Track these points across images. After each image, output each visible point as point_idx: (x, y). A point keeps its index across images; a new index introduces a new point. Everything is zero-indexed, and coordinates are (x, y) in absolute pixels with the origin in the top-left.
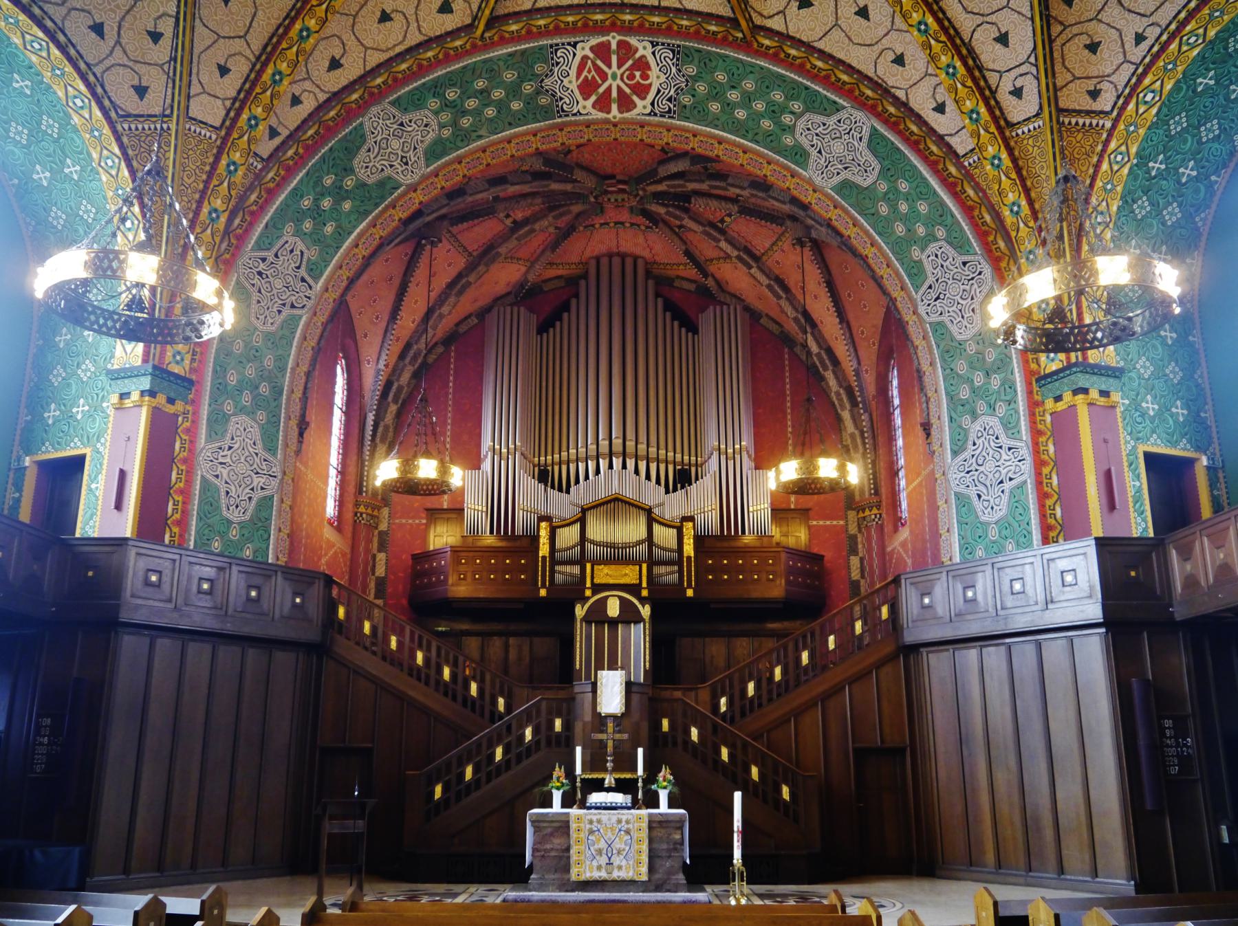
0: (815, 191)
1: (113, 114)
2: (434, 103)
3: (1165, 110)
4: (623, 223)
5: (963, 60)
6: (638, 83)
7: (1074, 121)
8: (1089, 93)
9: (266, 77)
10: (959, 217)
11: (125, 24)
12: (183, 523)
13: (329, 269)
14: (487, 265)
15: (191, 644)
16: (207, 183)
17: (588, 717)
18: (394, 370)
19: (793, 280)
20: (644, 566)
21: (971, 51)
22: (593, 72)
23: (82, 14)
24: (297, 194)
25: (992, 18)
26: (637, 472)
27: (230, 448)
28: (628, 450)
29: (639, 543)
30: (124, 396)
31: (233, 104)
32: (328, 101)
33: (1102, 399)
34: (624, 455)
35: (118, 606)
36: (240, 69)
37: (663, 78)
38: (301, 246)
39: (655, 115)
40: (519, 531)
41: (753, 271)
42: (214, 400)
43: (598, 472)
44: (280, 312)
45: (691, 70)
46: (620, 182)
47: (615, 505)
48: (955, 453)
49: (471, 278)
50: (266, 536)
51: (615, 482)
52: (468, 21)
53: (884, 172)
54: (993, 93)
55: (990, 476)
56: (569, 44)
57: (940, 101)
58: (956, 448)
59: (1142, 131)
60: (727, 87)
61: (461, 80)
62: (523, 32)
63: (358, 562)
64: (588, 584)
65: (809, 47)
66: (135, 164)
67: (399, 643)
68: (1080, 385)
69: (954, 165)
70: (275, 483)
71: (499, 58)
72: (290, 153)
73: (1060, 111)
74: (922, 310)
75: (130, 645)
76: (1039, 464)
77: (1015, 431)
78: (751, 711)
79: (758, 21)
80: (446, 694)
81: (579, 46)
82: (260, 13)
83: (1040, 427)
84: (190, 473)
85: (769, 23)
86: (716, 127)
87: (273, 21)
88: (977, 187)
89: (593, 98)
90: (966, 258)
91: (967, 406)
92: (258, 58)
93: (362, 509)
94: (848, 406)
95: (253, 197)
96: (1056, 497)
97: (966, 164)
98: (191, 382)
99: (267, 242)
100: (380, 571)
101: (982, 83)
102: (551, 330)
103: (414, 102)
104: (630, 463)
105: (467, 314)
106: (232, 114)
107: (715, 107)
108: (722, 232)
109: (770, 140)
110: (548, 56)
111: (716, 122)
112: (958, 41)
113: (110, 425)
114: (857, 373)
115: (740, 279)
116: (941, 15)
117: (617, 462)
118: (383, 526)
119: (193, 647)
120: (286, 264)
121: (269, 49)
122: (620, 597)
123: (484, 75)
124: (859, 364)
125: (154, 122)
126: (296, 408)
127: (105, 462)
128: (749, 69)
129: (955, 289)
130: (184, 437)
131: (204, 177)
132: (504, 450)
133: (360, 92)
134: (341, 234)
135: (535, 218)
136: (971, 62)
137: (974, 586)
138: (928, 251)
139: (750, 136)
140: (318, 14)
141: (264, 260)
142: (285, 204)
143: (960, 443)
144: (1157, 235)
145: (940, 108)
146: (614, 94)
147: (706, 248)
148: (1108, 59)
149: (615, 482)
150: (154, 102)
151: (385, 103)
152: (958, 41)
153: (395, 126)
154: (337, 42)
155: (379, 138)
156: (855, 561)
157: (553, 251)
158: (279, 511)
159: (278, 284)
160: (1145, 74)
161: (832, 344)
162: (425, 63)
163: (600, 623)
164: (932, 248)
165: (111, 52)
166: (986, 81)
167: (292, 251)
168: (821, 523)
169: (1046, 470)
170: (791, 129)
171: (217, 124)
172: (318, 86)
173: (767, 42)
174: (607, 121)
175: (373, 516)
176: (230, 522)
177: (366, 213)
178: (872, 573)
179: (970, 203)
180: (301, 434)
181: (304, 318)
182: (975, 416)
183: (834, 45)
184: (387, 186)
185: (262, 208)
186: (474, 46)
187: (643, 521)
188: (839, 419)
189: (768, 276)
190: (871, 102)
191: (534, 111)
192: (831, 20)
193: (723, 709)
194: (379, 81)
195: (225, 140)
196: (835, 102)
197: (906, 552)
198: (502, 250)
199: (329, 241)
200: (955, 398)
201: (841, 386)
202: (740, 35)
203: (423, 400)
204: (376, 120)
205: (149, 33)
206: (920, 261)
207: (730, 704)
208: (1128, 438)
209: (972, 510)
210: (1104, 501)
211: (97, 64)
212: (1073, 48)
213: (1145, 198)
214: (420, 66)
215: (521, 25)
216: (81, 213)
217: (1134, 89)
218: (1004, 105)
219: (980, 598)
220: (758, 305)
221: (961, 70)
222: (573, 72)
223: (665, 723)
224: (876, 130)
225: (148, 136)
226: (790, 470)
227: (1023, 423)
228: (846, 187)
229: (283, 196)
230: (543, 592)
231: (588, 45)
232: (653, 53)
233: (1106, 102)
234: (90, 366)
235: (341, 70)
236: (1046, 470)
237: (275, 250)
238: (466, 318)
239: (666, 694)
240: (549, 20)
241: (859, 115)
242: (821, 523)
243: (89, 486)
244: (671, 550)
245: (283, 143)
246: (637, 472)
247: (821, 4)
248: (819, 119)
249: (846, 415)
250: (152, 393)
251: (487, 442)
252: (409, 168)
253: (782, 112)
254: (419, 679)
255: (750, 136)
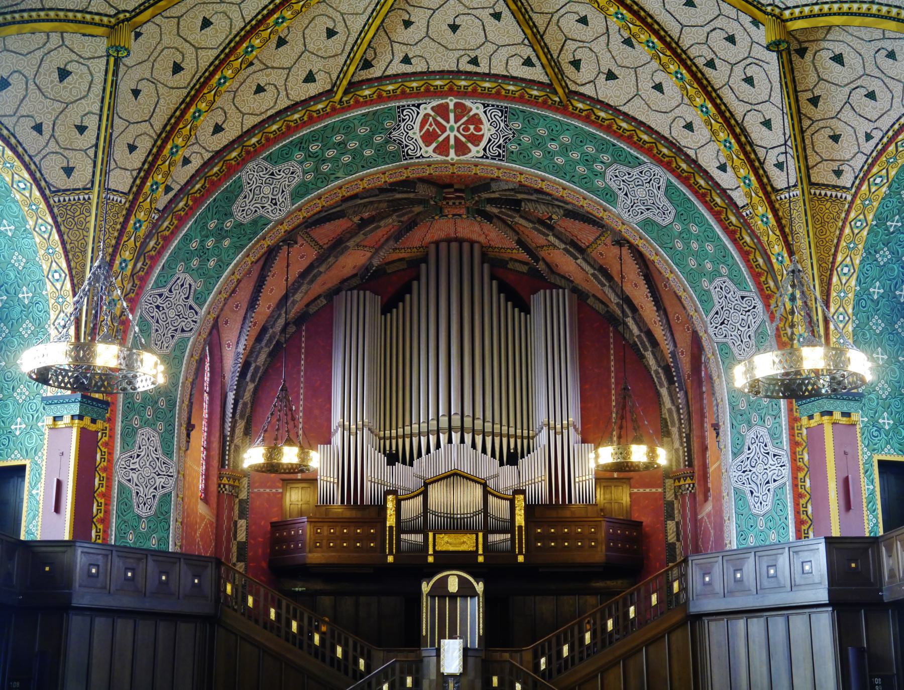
0: (623, 224)
1: (47, 192)
2: (299, 155)
3: (895, 185)
4: (460, 215)
5: (737, 137)
6: (472, 133)
7: (823, 193)
8: (834, 171)
9: (166, 152)
10: (737, 259)
11: (59, 122)
12: (105, 521)
13: (211, 296)
14: (336, 257)
15: (119, 620)
16: (119, 239)
17: (433, 676)
18: (252, 352)
19: (614, 271)
20: (481, 535)
21: (743, 130)
22: (434, 126)
23: (28, 119)
24: (187, 238)
25: (759, 107)
26: (474, 446)
27: (138, 456)
28: (465, 426)
29: (476, 514)
30: (55, 419)
31: (139, 173)
32: (211, 159)
33: (845, 419)
34: (462, 429)
35: (71, 594)
36: (145, 145)
37: (493, 131)
38: (189, 280)
39: (487, 158)
40: (367, 501)
41: (579, 261)
42: (125, 417)
43: (438, 446)
44: (173, 336)
45: (517, 125)
46: (457, 191)
47: (454, 476)
48: (735, 455)
49: (322, 269)
50: (166, 527)
51: (454, 455)
52: (329, 87)
53: (678, 215)
54: (762, 164)
55: (760, 476)
56: (413, 105)
57: (412, 61)
58: (735, 451)
59: (876, 204)
60: (547, 140)
61: (322, 137)
62: (375, 96)
63: (221, 530)
64: (431, 551)
65: (616, 111)
66: (62, 228)
67: (278, 615)
68: (825, 409)
69: (734, 214)
70: (172, 481)
71: (355, 118)
72: (181, 204)
73: (812, 184)
74: (711, 331)
75: (77, 623)
76: (795, 470)
77: (779, 441)
78: (566, 668)
79: (573, 87)
80: (316, 656)
81: (421, 107)
82: (162, 101)
83: (798, 439)
84: (109, 479)
85: (582, 90)
86: (539, 169)
87: (171, 106)
88: (753, 234)
89: (434, 145)
90: (744, 294)
91: (745, 416)
92: (159, 136)
93: (225, 481)
94: (665, 384)
95: (152, 243)
96: (808, 496)
97: (744, 214)
98: (107, 403)
99: (163, 281)
100: (242, 536)
101: (753, 156)
102: (395, 310)
103: (284, 156)
104: (468, 438)
105: (316, 295)
106: (138, 182)
107: (537, 154)
108: (551, 228)
109: (584, 181)
110: (397, 115)
111: (539, 165)
112: (733, 122)
113: (46, 442)
114: (673, 355)
115: (569, 265)
116: (718, 101)
117: (456, 437)
118: (243, 495)
119: (120, 623)
120: (178, 297)
121: (168, 128)
122: (458, 576)
123: (342, 131)
124: (675, 346)
125: (78, 194)
126: (185, 415)
127: (43, 472)
128: (566, 127)
129: (736, 318)
130: (103, 449)
131: (116, 234)
132: (353, 427)
133: (239, 150)
134: (221, 266)
135: (381, 216)
136: (743, 139)
137: (741, 570)
138: (715, 283)
139: (568, 177)
140: (208, 99)
141: (161, 295)
142: (178, 248)
143: (738, 447)
144: (898, 276)
145: (723, 168)
146: (452, 142)
147: (537, 238)
148: (846, 149)
149: (454, 455)
150: (80, 178)
151: (259, 160)
152: (733, 122)
153: (267, 176)
154: (220, 112)
155: (254, 187)
156: (671, 525)
157: (396, 241)
158: (176, 505)
159: (172, 314)
160: (872, 165)
161: (651, 327)
162: (292, 124)
163: (442, 597)
164: (718, 282)
165: (47, 144)
166: (756, 154)
167: (182, 285)
168: (641, 490)
169: (801, 475)
170: (603, 175)
171: (126, 190)
172: (204, 148)
173: (580, 105)
174: (446, 162)
175: (233, 487)
176: (140, 517)
177: (242, 247)
178: (686, 542)
179: (747, 248)
180: (188, 435)
181: (192, 340)
182: (750, 426)
183: (635, 109)
184: (258, 223)
185: (160, 253)
186: (334, 109)
187: (478, 491)
188: (658, 395)
189: (592, 266)
190: (667, 159)
191: (382, 156)
192: (633, 91)
193: (543, 667)
194: (254, 140)
195: (133, 203)
196: (637, 158)
197: (710, 523)
198: (351, 243)
199: (211, 273)
200: (736, 408)
201: (659, 366)
202: (557, 99)
203: (277, 377)
204: (252, 174)
205: (77, 127)
206: (709, 291)
207: (548, 663)
208: (865, 450)
209: (746, 504)
210: (842, 502)
211: (37, 155)
212: (821, 137)
213: (885, 249)
214: (288, 127)
215: (374, 90)
216: (13, 261)
217: (865, 175)
218: (770, 174)
219: (745, 579)
220: (585, 286)
221: (735, 146)
222: (417, 126)
223: (495, 680)
224: (671, 183)
225: (73, 205)
226: (607, 454)
227: (784, 435)
228: (647, 224)
229: (176, 242)
230: (390, 559)
231: (429, 106)
232: (485, 112)
233: (847, 180)
234: (24, 390)
235: (222, 133)
236: (801, 475)
237: (169, 286)
238: (316, 299)
239: (497, 656)
240: (397, 85)
241: (658, 170)
242: (641, 490)
243: (30, 492)
244: (504, 521)
245: (175, 196)
246: (474, 446)
247: (624, 78)
248: (625, 169)
249: (664, 392)
250: (80, 417)
251: (336, 418)
252: (278, 207)
253: (594, 161)
254: (294, 644)
255: (568, 177)
